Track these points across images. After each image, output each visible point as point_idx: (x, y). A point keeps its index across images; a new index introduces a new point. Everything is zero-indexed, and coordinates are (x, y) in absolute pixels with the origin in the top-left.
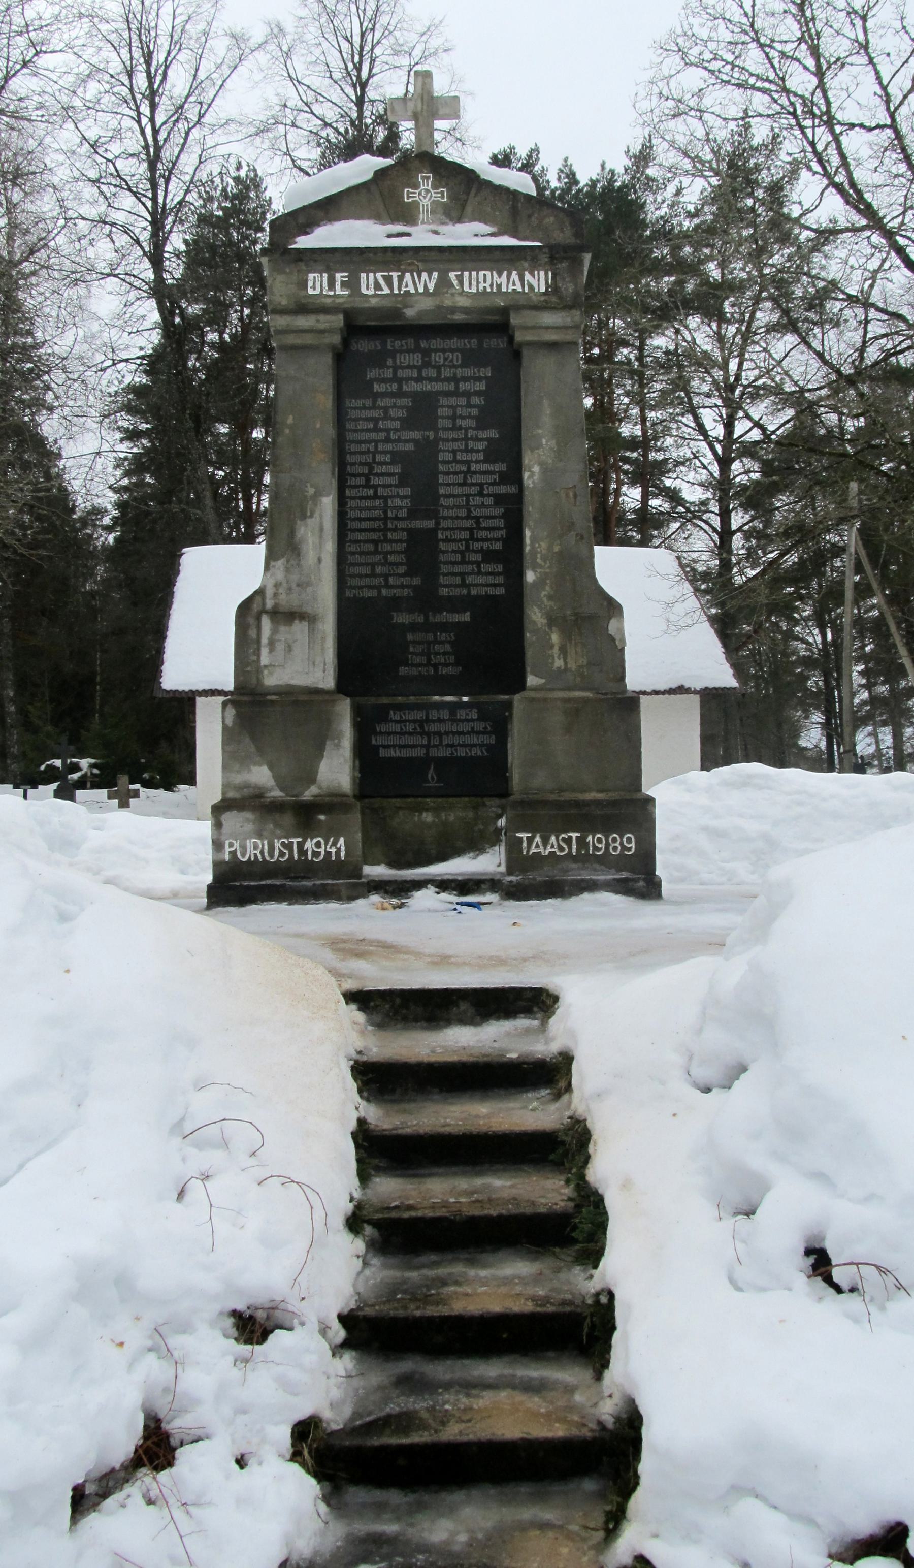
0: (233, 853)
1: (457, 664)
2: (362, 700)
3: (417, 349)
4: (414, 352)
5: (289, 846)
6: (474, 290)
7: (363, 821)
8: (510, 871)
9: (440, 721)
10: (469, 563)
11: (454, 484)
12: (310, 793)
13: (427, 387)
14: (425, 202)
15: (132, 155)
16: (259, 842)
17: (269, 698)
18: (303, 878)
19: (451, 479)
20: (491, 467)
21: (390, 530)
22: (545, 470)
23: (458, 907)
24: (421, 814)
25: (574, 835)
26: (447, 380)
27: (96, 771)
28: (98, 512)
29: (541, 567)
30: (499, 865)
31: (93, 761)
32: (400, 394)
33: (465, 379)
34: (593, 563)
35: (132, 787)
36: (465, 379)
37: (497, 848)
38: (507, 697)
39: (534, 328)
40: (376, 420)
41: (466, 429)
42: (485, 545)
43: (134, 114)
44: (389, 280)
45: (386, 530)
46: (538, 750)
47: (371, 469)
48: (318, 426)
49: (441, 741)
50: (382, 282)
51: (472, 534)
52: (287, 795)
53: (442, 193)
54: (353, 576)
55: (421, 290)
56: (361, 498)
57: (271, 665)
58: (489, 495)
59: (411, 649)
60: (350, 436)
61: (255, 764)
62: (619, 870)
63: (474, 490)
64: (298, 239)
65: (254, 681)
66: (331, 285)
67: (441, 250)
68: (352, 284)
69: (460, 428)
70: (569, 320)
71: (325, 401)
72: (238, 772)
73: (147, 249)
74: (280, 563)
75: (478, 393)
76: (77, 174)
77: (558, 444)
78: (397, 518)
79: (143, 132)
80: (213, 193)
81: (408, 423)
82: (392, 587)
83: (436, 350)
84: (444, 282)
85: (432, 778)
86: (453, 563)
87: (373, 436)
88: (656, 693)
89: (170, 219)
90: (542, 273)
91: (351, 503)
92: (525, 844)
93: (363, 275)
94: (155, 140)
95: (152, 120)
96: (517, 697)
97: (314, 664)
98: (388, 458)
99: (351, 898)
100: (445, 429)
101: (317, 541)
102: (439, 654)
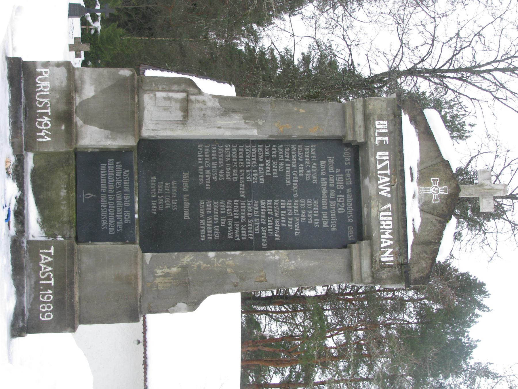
0: (41, 74)
1: (158, 212)
2: (135, 154)
3: (346, 187)
4: (344, 185)
5: (45, 107)
6: (381, 218)
7: (61, 153)
8: (29, 242)
9: (123, 200)
10: (219, 218)
11: (266, 209)
12: (78, 120)
13: (324, 193)
14: (432, 190)
15: (474, 58)
16: (48, 89)
17: (136, 97)
18: (26, 115)
19: (270, 207)
20: (277, 231)
21: (239, 171)
22: (276, 263)
23: (7, 208)
24: (65, 189)
25: (52, 282)
26: (328, 205)
27: (93, 32)
28: (257, 39)
29: (218, 261)
30: (33, 236)
31: (99, 30)
32: (319, 177)
33: (329, 215)
34: (221, 293)
35: (82, 53)
36: (329, 215)
37: (44, 235)
38: (138, 242)
39: (360, 255)
40: (303, 162)
41: (299, 216)
42: (230, 228)
43: (499, 58)
44: (385, 168)
45: (239, 169)
46: (106, 261)
47: (275, 159)
48: (299, 127)
49: (111, 201)
50: (384, 164)
51: (237, 220)
52: (76, 107)
53: (437, 200)
54: (210, 149)
55: (380, 187)
56: (257, 154)
57: (156, 98)
58: (260, 230)
59: (166, 184)
60: (294, 147)
61: (96, 87)
62: (30, 310)
63: (263, 221)
64: (407, 116)
65: (146, 88)
66: (381, 134)
67: (404, 198)
68: (382, 147)
69: (300, 213)
70: (366, 276)
71: (314, 132)
72: (91, 77)
73: (418, 66)
74: (217, 104)
75: (321, 223)
76: (462, 24)
77: (292, 270)
78: (246, 175)
79: (488, 64)
80: (455, 109)
81: (302, 182)
82: (204, 173)
83: (345, 198)
84: (384, 200)
85: (88, 196)
86: (219, 209)
87: (294, 161)
88: (145, 380)
89: (437, 81)
90: (392, 259)
91: (254, 147)
92: (46, 251)
93: (387, 153)
94: (484, 71)
95: (496, 69)
96: (138, 246)
97: (156, 124)
98: (281, 170)
99: (13, 145)
100: (299, 204)
101: (231, 126)
102: (164, 200)
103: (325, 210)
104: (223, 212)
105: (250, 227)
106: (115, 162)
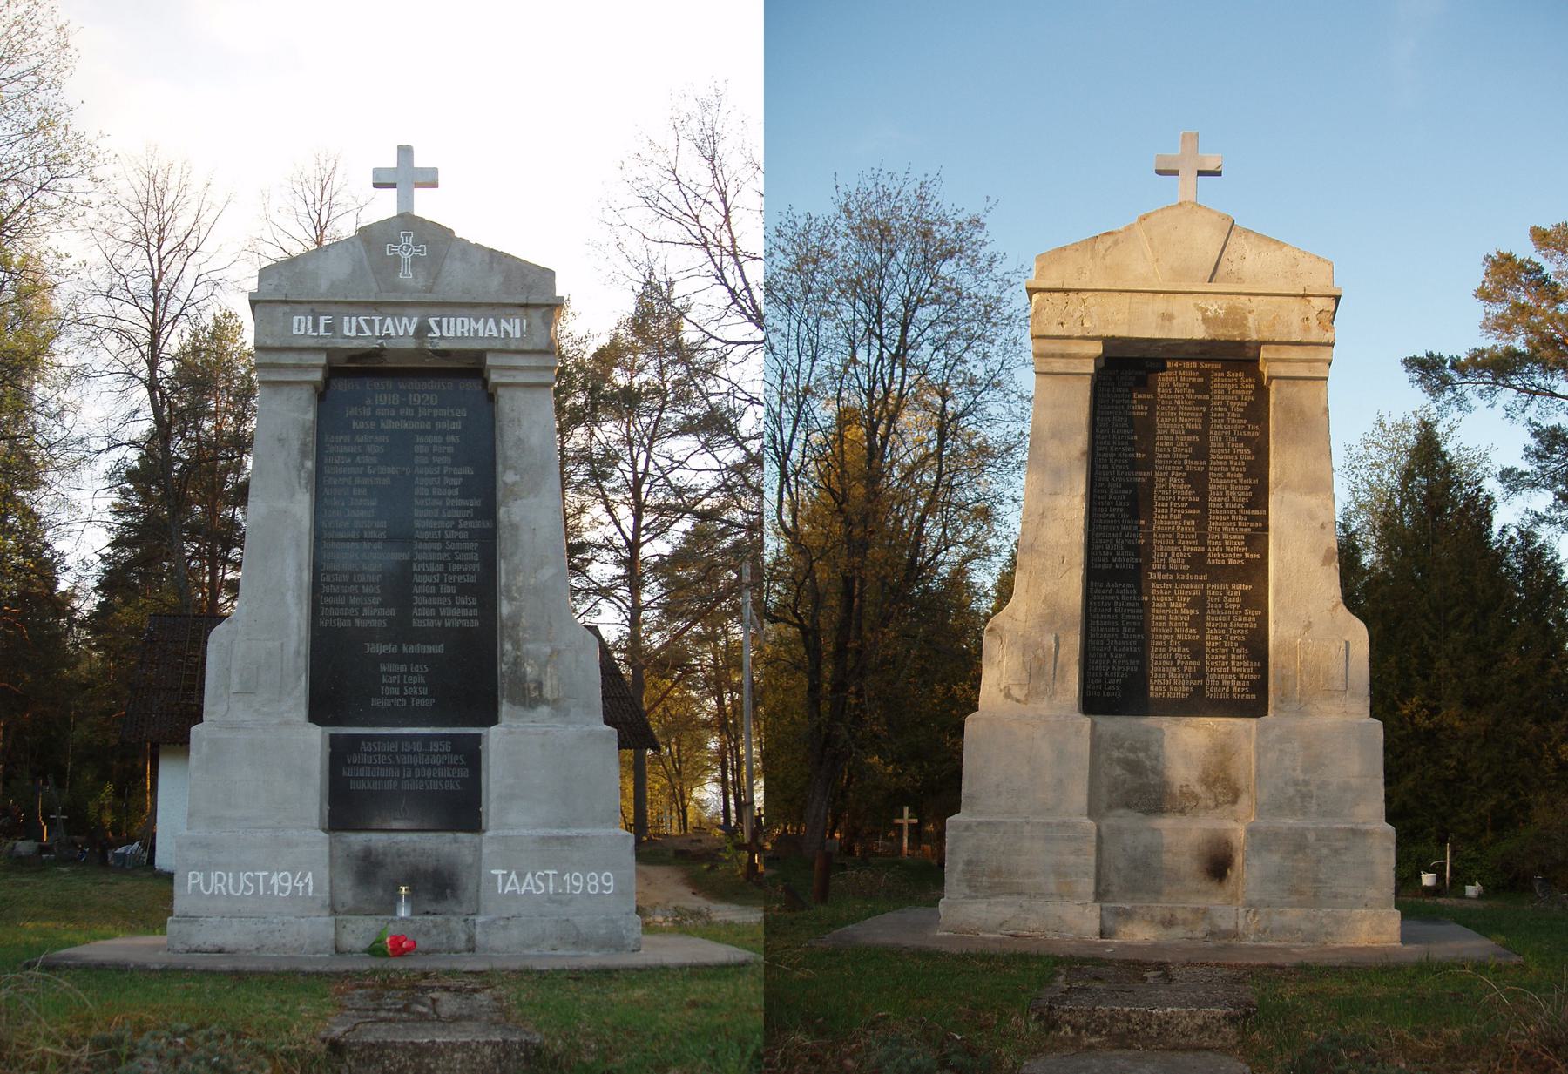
9: (412, 753)
14: (406, 256)
25: (551, 873)
26: (424, 419)
33: (441, 419)
36: (441, 419)
42: (460, 578)
44: (370, 323)
50: (363, 324)
51: (446, 568)
66: (316, 327)
69: (436, 464)
75: (453, 432)
86: (428, 596)
87: (351, 470)
100: (421, 466)
103: (433, 426)
104: (433, 590)
105: (458, 546)
106: (347, 765)
